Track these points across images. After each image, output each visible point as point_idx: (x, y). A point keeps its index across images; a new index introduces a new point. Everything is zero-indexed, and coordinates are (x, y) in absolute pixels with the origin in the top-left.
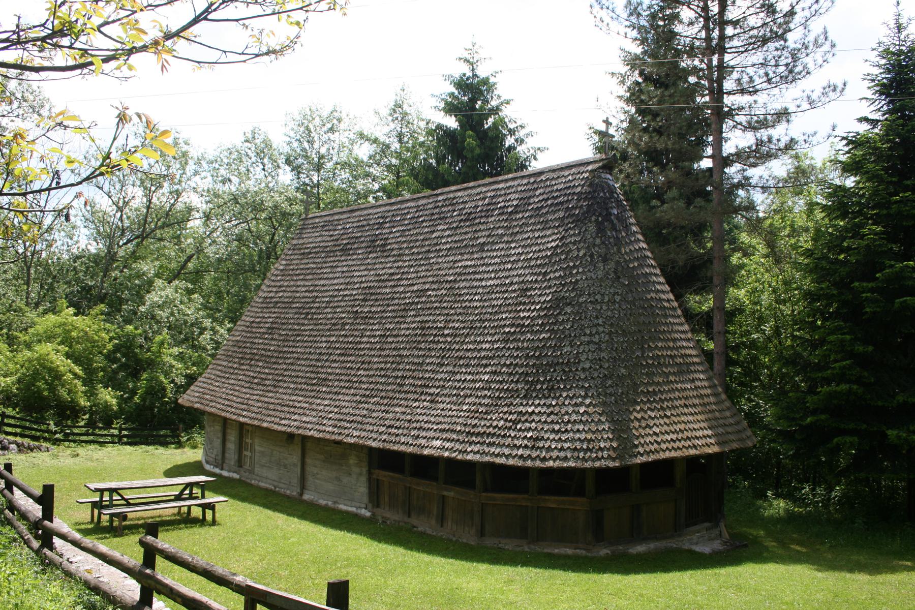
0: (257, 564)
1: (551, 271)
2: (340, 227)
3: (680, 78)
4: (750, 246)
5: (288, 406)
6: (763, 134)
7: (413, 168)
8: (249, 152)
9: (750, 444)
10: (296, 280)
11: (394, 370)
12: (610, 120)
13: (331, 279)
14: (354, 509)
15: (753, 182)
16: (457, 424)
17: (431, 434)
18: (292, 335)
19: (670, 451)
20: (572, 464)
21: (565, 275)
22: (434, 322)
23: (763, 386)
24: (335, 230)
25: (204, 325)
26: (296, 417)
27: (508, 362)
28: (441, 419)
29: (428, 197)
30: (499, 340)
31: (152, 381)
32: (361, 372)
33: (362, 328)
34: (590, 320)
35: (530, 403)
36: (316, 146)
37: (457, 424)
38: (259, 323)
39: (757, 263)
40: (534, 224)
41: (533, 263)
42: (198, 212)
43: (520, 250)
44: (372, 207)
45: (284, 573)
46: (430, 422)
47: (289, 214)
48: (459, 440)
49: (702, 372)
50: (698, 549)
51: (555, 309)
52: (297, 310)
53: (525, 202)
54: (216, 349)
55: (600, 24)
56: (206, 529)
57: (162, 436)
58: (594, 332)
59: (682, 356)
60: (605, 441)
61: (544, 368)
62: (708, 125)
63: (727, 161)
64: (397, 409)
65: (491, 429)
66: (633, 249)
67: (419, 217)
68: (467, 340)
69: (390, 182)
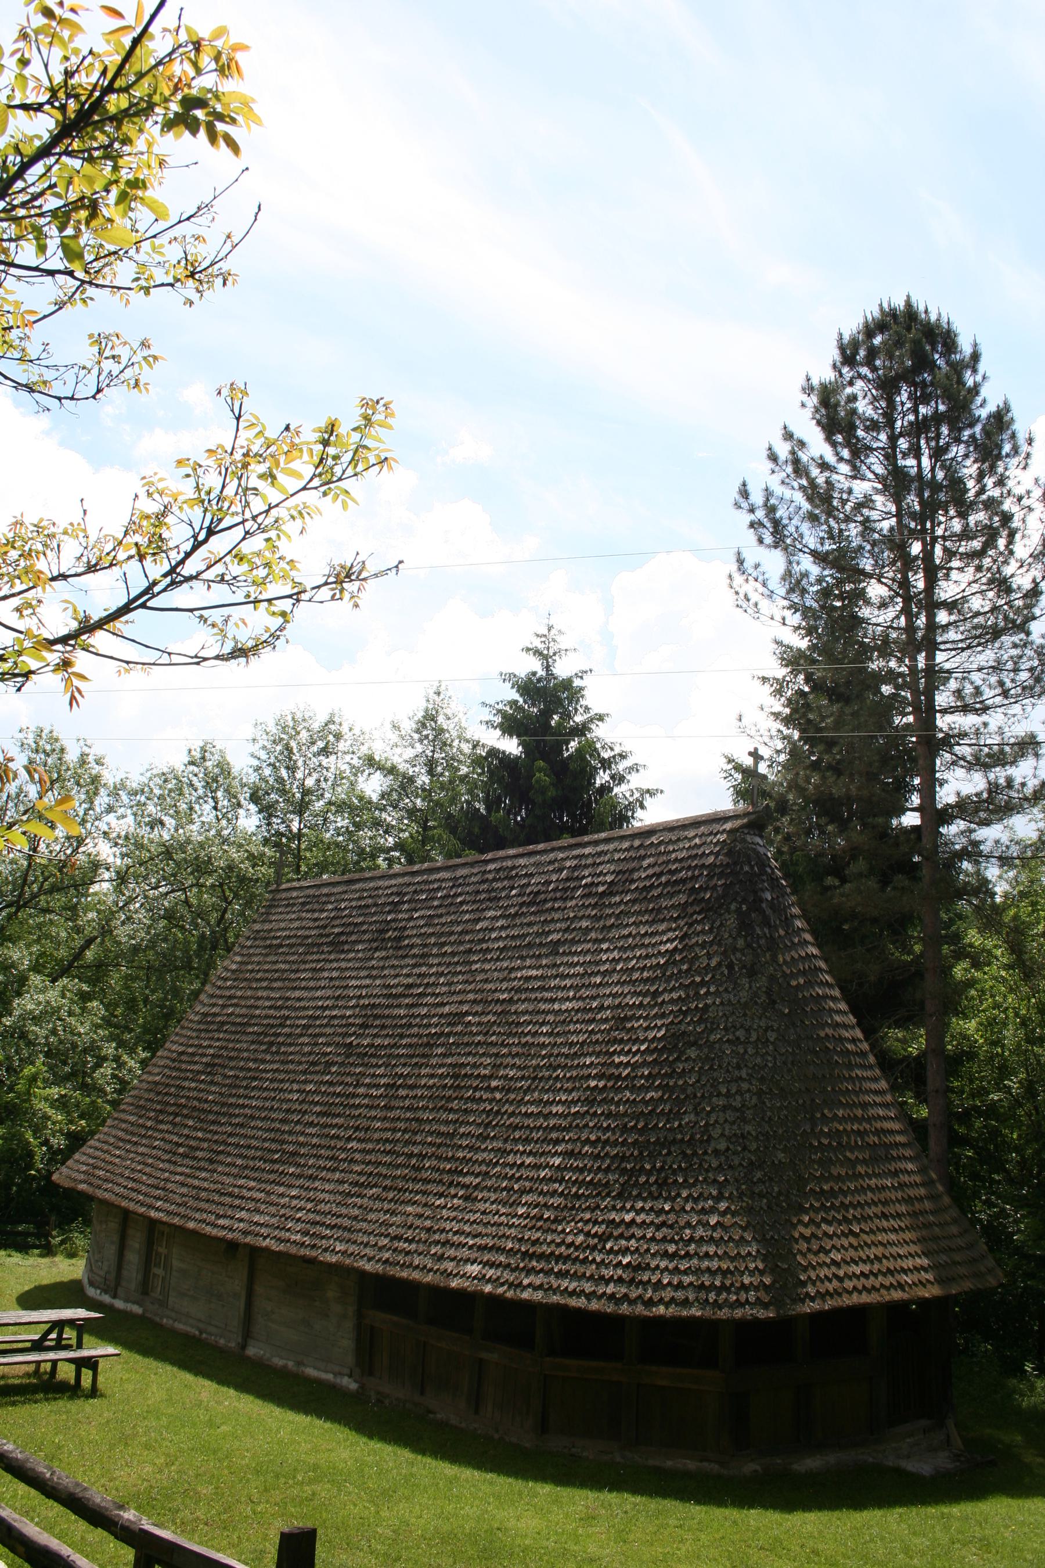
0: (160, 1471)
1: (665, 990)
2: (330, 907)
3: (868, 687)
4: (983, 950)
5: (230, 1195)
6: (999, 774)
7: (450, 816)
8: (195, 779)
9: (992, 1282)
10: (256, 989)
11: (407, 1143)
12: (760, 752)
13: (312, 989)
14: (330, 1377)
15: (985, 848)
16: (508, 1237)
17: (465, 1253)
18: (245, 1078)
19: (860, 1292)
20: (696, 1312)
21: (688, 996)
22: (475, 1066)
23: (1010, 1180)
24: (322, 911)
25: (103, 1053)
26: (243, 1214)
27: (593, 1137)
28: (480, 1229)
29: (472, 865)
30: (579, 1100)
31: (12, 1140)
32: (353, 1144)
33: (358, 1071)
34: (728, 1071)
35: (628, 1206)
36: (299, 775)
37: (508, 1237)
38: (193, 1054)
39: (995, 978)
40: (639, 913)
41: (636, 976)
42: (108, 869)
43: (616, 954)
44: (382, 877)
45: (206, 1490)
46: (463, 1233)
47: (251, 880)
48: (509, 1265)
49: (910, 1159)
50: (911, 1466)
51: (670, 1052)
52: (255, 1037)
53: (625, 876)
54: (119, 1092)
55: (745, 605)
56: (80, 1402)
57: (20, 1233)
58: (733, 1091)
59: (878, 1132)
60: (752, 1273)
61: (652, 1148)
62: (913, 760)
63: (945, 816)
64: (410, 1209)
65: (563, 1248)
66: (796, 956)
67: (456, 895)
68: (527, 1098)
69: (411, 836)
